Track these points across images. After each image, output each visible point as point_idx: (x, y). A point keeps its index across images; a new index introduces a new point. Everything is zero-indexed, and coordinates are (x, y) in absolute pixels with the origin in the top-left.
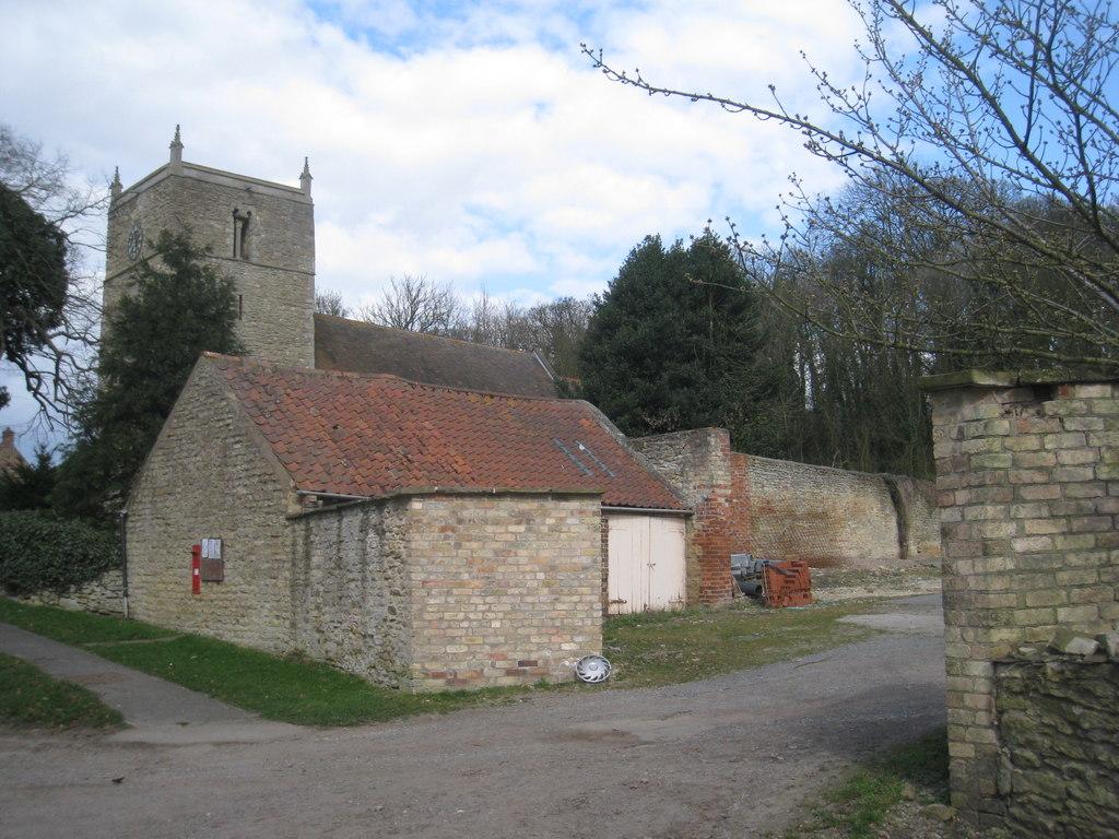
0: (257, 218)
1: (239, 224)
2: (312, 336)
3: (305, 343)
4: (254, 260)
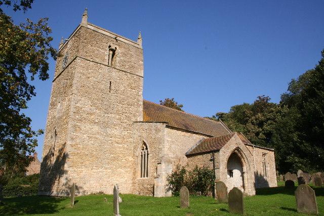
0: (119, 51)
1: (111, 52)
2: (142, 103)
3: (138, 105)
4: (117, 67)
